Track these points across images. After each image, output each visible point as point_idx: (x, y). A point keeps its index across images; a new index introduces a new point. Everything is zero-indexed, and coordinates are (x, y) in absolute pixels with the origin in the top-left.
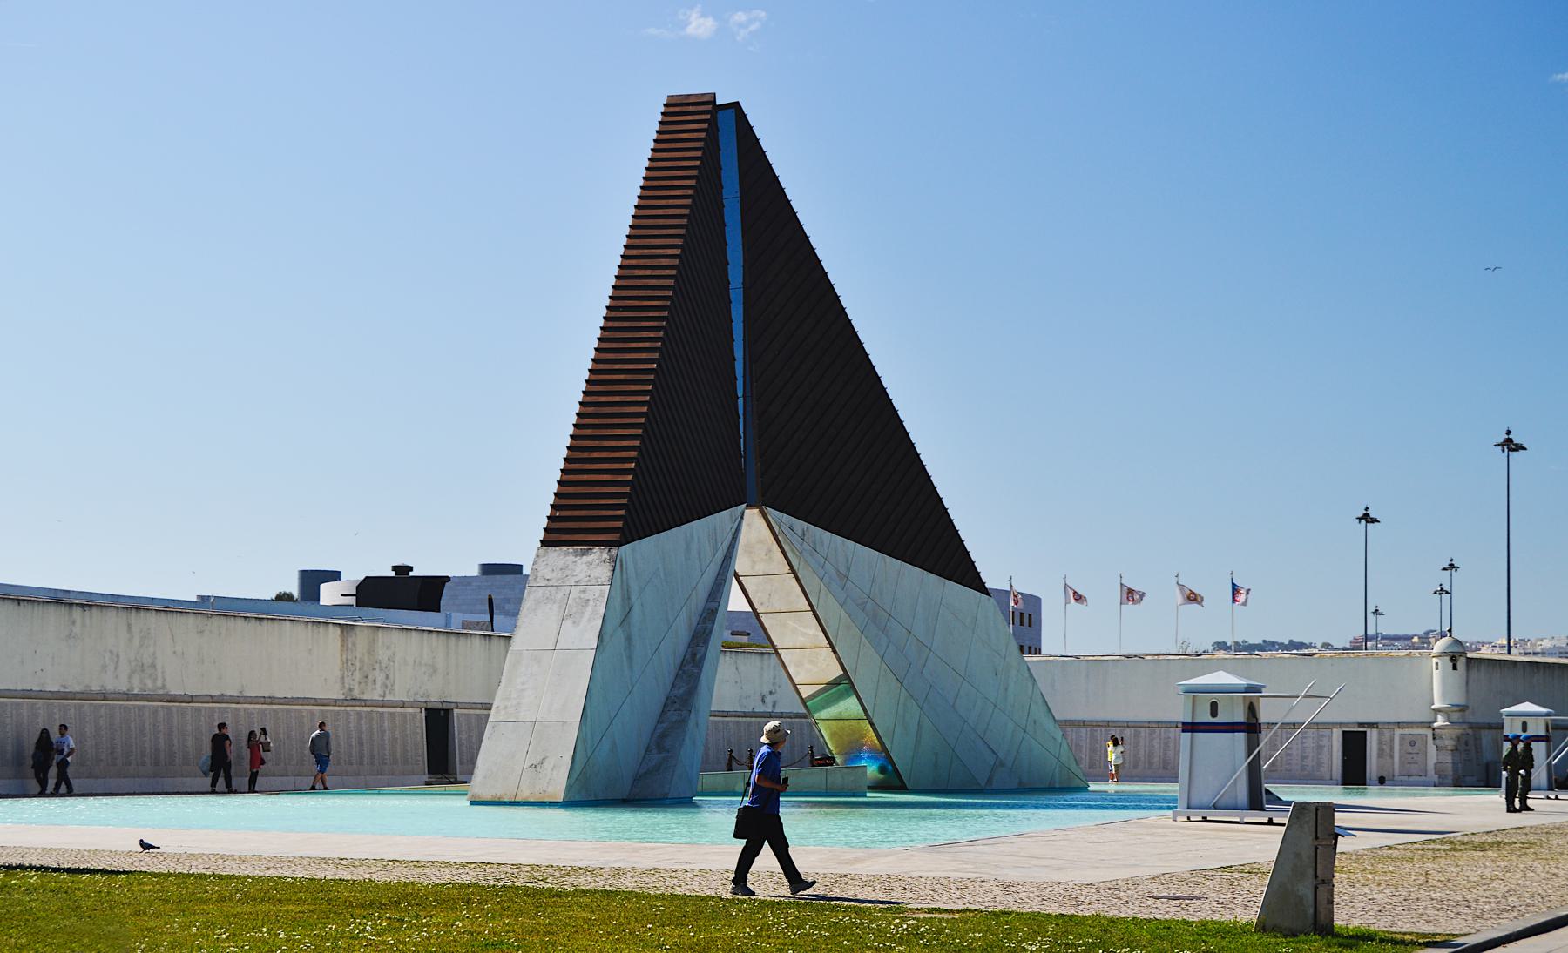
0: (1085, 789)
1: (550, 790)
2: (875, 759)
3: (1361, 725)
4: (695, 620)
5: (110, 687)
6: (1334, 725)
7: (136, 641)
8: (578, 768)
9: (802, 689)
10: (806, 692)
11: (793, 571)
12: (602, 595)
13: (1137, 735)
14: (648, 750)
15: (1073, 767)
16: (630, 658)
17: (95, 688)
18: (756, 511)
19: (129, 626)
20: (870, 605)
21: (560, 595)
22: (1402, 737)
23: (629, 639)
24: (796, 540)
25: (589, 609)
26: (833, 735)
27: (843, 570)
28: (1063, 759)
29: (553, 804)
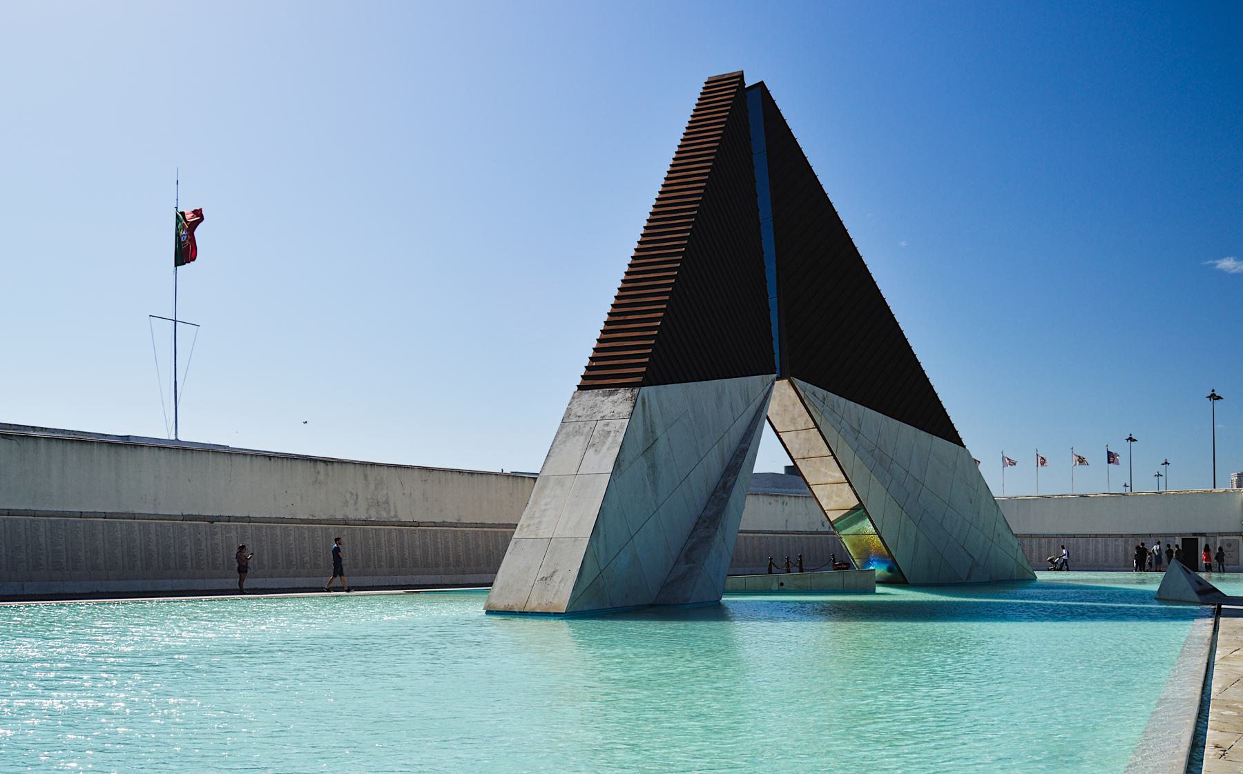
0: (1021, 580)
1: (556, 601)
2: (885, 562)
3: (1194, 534)
4: (728, 457)
5: (351, 516)
6: (1176, 535)
7: (372, 487)
8: (586, 582)
9: (830, 514)
10: (833, 516)
11: (817, 426)
12: (621, 427)
13: (1049, 543)
14: (677, 562)
15: (1025, 563)
16: (654, 484)
17: (339, 516)
18: (786, 381)
19: (366, 476)
20: (877, 451)
21: (587, 429)
22: (1222, 541)
23: (653, 467)
24: (819, 404)
25: (610, 439)
26: (854, 545)
27: (855, 426)
28: (1019, 560)
29: (557, 615)
